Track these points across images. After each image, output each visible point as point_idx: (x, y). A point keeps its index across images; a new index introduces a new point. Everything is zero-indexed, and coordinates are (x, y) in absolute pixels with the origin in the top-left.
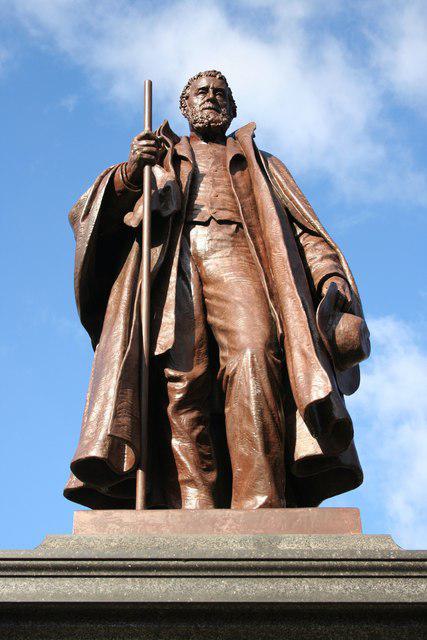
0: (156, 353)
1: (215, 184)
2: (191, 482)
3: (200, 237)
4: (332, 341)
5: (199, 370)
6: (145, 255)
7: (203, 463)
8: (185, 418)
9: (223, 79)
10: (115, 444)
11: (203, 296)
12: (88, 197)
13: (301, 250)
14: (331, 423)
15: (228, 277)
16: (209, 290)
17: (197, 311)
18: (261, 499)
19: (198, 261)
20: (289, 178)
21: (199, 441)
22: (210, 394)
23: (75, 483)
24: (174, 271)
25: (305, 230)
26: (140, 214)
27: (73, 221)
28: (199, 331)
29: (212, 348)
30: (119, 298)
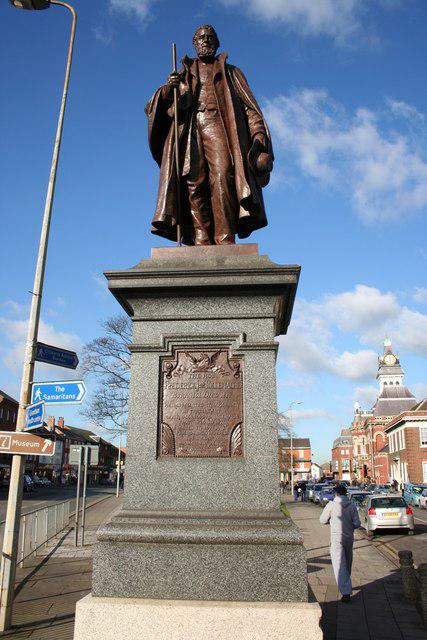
0: (184, 174)
1: (207, 90)
2: (199, 228)
3: (201, 117)
4: (255, 166)
5: (201, 180)
6: (176, 129)
7: (203, 221)
8: (196, 201)
9: (212, 30)
10: (167, 217)
11: (203, 145)
12: (152, 98)
13: (246, 118)
14: (255, 204)
15: (213, 137)
16: (205, 143)
17: (200, 152)
18: (225, 236)
19: (201, 128)
20: (176, 521)
21: (202, 211)
22: (206, 191)
23: (155, 229)
24: (189, 136)
25: (249, 108)
26: (173, 111)
27: (146, 111)
28: (201, 162)
29: (207, 171)
30: (167, 149)
